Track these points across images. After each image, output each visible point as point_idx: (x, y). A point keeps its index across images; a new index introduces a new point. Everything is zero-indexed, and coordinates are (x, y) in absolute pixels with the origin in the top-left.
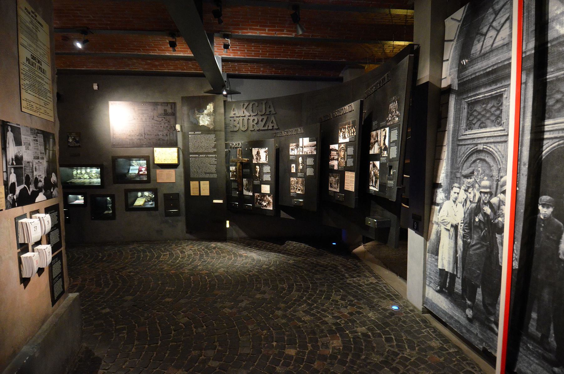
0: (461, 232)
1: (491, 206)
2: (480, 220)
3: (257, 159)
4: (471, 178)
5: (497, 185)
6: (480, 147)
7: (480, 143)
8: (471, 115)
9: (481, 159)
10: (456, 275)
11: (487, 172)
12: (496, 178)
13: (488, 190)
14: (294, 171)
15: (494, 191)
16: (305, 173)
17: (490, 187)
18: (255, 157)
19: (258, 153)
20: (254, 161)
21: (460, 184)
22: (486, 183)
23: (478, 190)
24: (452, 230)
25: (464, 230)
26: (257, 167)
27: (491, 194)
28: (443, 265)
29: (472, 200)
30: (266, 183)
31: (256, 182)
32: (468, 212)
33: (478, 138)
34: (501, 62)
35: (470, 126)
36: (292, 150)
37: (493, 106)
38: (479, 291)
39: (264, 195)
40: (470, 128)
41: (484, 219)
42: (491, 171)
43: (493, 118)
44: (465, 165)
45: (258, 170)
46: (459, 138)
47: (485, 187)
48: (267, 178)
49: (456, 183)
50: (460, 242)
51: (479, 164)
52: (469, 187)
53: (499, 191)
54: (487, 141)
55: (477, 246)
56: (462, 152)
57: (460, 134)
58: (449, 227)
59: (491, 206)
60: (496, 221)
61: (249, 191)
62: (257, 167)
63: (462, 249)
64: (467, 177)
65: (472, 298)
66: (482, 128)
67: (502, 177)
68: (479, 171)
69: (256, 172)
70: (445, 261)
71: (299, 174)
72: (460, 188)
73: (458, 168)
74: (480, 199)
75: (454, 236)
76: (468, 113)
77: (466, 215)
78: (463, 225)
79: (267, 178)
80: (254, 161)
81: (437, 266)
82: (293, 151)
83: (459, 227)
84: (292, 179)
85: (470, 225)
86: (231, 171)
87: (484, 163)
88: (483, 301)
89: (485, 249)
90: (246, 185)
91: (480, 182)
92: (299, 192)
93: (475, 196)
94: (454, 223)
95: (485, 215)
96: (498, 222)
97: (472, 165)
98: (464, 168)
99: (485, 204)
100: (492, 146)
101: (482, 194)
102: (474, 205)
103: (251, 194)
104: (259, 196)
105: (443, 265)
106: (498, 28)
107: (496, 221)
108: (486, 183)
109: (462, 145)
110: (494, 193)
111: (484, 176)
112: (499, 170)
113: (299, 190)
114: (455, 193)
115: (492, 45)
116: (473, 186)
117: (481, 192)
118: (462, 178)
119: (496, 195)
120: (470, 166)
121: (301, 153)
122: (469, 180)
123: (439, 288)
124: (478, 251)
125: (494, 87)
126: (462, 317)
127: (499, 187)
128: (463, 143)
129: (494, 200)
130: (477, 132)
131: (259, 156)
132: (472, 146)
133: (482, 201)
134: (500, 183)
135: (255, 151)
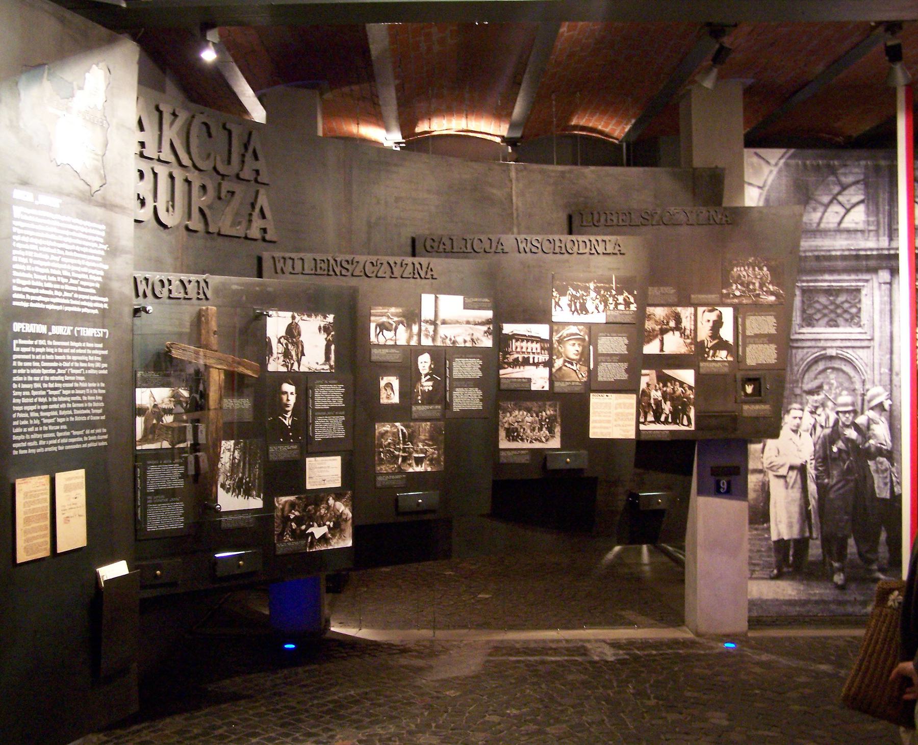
0: (811, 471)
1: (857, 427)
2: (839, 450)
3: (287, 354)
4: (818, 394)
5: (863, 400)
6: (833, 352)
7: (832, 347)
8: (810, 306)
9: (833, 369)
10: (811, 537)
11: (846, 384)
12: (860, 391)
13: (850, 408)
14: (395, 399)
15: (859, 409)
16: (447, 405)
17: (853, 404)
18: (277, 349)
19: (292, 333)
20: (275, 365)
21: (801, 404)
22: (845, 398)
23: (832, 409)
24: (793, 475)
25: (816, 469)
26: (288, 388)
27: (855, 412)
28: (779, 534)
29: (823, 424)
30: (326, 449)
31: (281, 451)
32: (820, 441)
33: (826, 340)
34: (855, 250)
35: (809, 321)
36: (382, 327)
37: (846, 301)
38: (851, 541)
39: (320, 496)
40: (810, 325)
41: (846, 446)
42: (852, 383)
43: (847, 316)
44: (806, 376)
45: (292, 399)
46: (792, 337)
47: (845, 405)
48: (329, 427)
49: (796, 402)
50: (812, 487)
51: (832, 377)
52: (816, 408)
53: (866, 407)
54: (842, 345)
55: (840, 485)
56: (799, 358)
57: (793, 331)
58: (783, 471)
59: (857, 427)
60: (867, 445)
61: (248, 494)
62: (288, 388)
63: (816, 496)
64: (811, 392)
65: (841, 554)
66: (831, 326)
67: (868, 390)
68: (832, 384)
69: (281, 408)
70: (783, 522)
71: (419, 409)
72: (802, 410)
73: (797, 381)
74: (837, 422)
75: (799, 481)
76: (803, 302)
77: (817, 447)
78: (813, 462)
79: (329, 427)
80: (275, 365)
81: (769, 538)
82: (389, 334)
83: (808, 466)
84: (383, 428)
85: (825, 458)
86: (142, 411)
87: (841, 374)
88: (860, 554)
89: (852, 484)
90: (234, 467)
91: (835, 398)
92: (419, 469)
93: (828, 418)
94: (798, 462)
95: (848, 440)
96: (869, 447)
97: (820, 376)
98: (806, 380)
99: (848, 426)
100: (850, 351)
101: (841, 415)
102: (827, 431)
103: (256, 503)
104: (293, 505)
105: (779, 534)
106: (848, 207)
107: (867, 445)
108: (845, 398)
109: (803, 348)
110: (859, 410)
111: (842, 390)
112: (864, 382)
113: (419, 461)
114: (795, 418)
115: (840, 223)
116: (823, 405)
117: (837, 413)
118: (804, 395)
119: (862, 413)
120: (816, 378)
121: (426, 342)
122: (816, 397)
123: (775, 571)
124: (841, 491)
125: (853, 277)
126: (828, 591)
127: (866, 403)
128: (799, 344)
129: (861, 420)
130: (821, 331)
131: (299, 345)
132: (816, 350)
133: (840, 424)
134: (867, 398)
135: (276, 324)
